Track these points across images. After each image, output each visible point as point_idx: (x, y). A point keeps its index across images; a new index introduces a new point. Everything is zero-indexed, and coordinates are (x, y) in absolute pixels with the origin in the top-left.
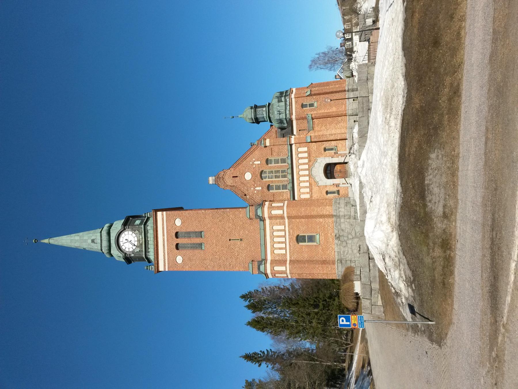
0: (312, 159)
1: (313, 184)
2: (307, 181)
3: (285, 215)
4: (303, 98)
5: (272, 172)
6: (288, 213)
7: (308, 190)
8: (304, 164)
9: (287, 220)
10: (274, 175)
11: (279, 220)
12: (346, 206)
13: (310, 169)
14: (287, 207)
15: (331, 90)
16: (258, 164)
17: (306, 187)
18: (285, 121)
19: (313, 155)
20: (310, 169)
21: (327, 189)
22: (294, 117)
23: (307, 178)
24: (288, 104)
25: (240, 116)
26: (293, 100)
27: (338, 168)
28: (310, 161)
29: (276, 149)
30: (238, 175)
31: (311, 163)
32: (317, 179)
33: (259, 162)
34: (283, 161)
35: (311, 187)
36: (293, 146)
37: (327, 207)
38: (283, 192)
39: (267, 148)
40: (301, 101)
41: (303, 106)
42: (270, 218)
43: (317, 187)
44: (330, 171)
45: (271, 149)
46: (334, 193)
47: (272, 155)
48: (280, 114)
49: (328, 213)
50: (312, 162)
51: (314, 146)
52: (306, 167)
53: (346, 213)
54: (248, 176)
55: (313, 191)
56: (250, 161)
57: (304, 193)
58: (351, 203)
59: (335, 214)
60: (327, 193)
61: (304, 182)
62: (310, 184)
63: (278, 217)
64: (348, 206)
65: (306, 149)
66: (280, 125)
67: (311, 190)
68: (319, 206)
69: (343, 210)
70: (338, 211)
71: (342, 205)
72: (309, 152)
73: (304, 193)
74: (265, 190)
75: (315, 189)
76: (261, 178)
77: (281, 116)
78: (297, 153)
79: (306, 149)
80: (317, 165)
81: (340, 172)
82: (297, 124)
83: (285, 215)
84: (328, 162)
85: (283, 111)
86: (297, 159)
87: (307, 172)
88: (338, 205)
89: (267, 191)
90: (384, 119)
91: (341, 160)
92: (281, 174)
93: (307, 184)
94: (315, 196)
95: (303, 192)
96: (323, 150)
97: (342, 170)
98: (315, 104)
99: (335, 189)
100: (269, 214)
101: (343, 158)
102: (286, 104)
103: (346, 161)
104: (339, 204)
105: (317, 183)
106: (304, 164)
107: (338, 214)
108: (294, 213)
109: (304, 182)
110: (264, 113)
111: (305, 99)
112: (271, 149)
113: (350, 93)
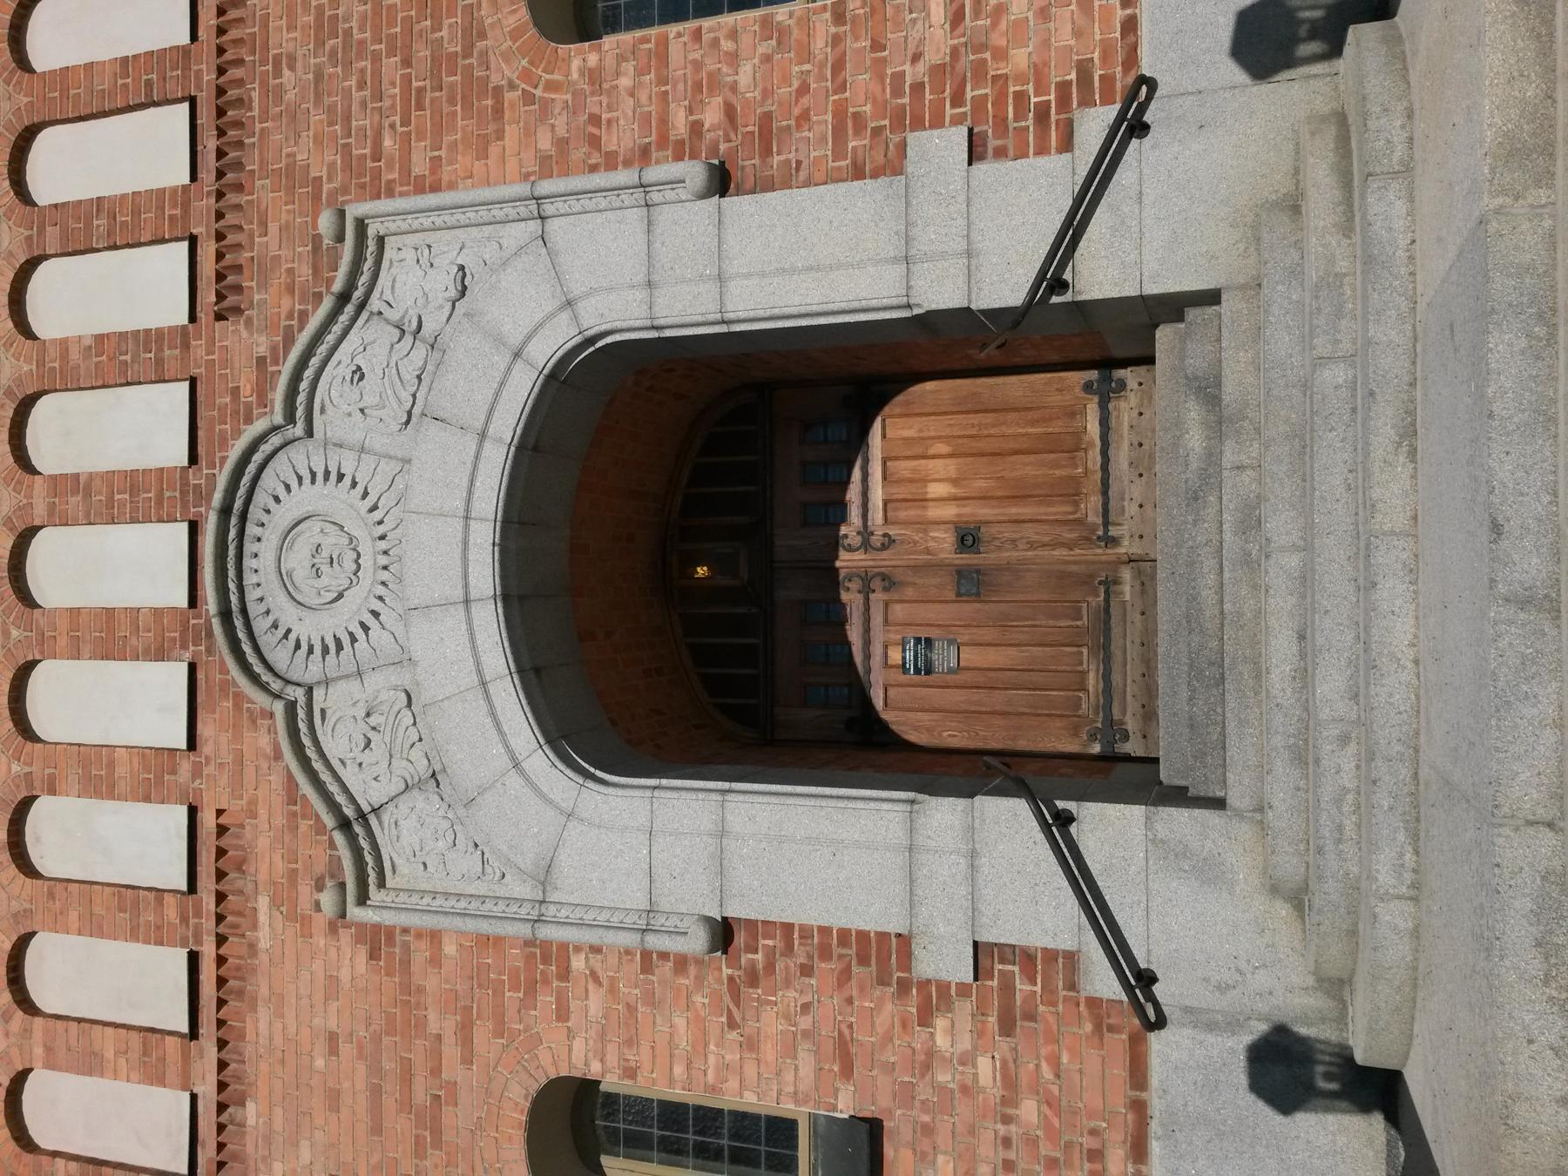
0: (277, 236)
1: (266, 850)
13: (219, 510)
15: (864, 303)
19: (293, 139)
27: (913, 479)
28: (219, 291)
31: (243, 342)
44: (695, 558)
55: (261, 1028)
62: (212, 851)
66: (1002, 1154)
67: (215, 993)
75: (305, 984)
80: (360, 387)
81: (971, 583)
84: (620, 312)
90: (1308, 636)
91: (944, 234)
97: (1026, 541)
101: (1035, 190)
103: (1100, 276)
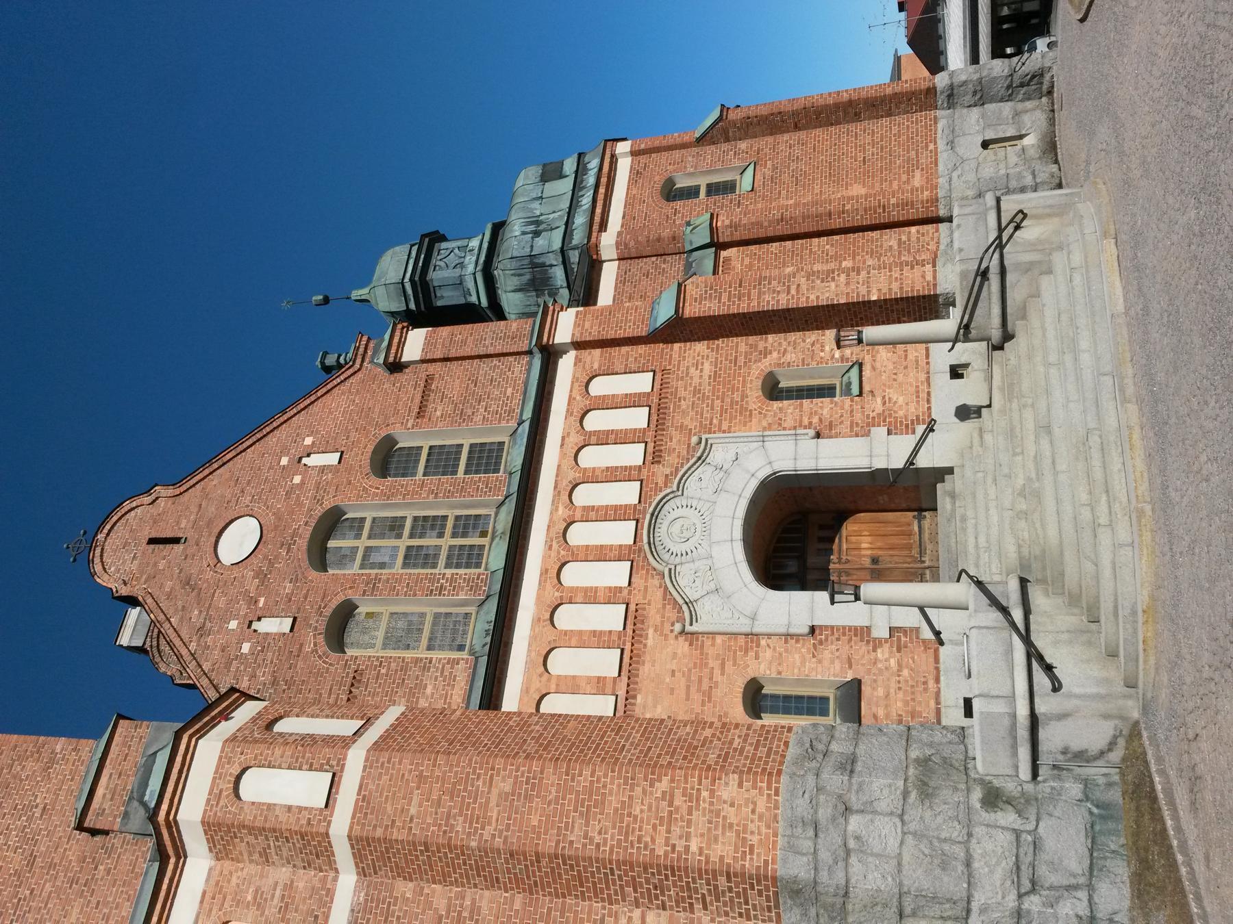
0: (675, 441)
1: (653, 614)
2: (612, 596)
3: (340, 825)
4: (677, 154)
5: (395, 527)
6: (364, 802)
7: (606, 662)
8: (614, 475)
9: (347, 883)
10: (404, 542)
11: (282, 874)
12: (926, 793)
13: (645, 516)
14: (377, 746)
16: (323, 469)
17: (598, 639)
18: (558, 274)
19: (684, 416)
20: (645, 516)
21: (762, 667)
22: (608, 242)
23: (616, 574)
24: (591, 180)
25: (357, 294)
26: (624, 166)
28: (655, 457)
29: (452, 380)
30: (182, 527)
31: (661, 471)
32: (689, 583)
33: (333, 458)
34: (485, 458)
35: (630, 643)
36: (566, 366)
37: (729, 789)
38: (426, 665)
39: (405, 377)
40: (662, 166)
41: (671, 193)
42: (222, 835)
43: (682, 646)
44: (796, 533)
45: (429, 380)
46: (812, 705)
47: (420, 415)
48: (537, 234)
49: (723, 850)
50: (670, 459)
51: (697, 360)
52: (627, 493)
53: (917, 878)
54: (239, 540)
55: (645, 670)
56: (284, 451)
57: (572, 686)
58: (980, 767)
59: (796, 868)
60: (756, 699)
61: (591, 596)
62: (634, 619)
63: (276, 833)
64: (949, 798)
65: (641, 383)
67: (630, 665)
68: (654, 769)
69: (882, 833)
70: (830, 840)
71: (882, 788)
72: (659, 405)
73: (572, 686)
74: (313, 640)
75: (664, 655)
76: (319, 556)
77: (540, 243)
78: (581, 403)
79: (641, 383)
80: (700, 483)
82: (621, 281)
83: (340, 825)
85: (559, 218)
86: (575, 439)
87: (622, 533)
88: (834, 780)
89: (323, 648)
91: (886, 452)
92: (447, 542)
93: (611, 618)
94: (650, 706)
95: (566, 666)
96: (754, 393)
98: (746, 183)
99: (822, 673)
100: (214, 796)
101: (909, 442)
102: (577, 186)
104: (849, 765)
105: (683, 609)
106: (614, 475)
107: (830, 880)
108: (417, 815)
109: (591, 596)
110: (470, 260)
111: (689, 155)
112: (429, 380)
113: (960, 112)
